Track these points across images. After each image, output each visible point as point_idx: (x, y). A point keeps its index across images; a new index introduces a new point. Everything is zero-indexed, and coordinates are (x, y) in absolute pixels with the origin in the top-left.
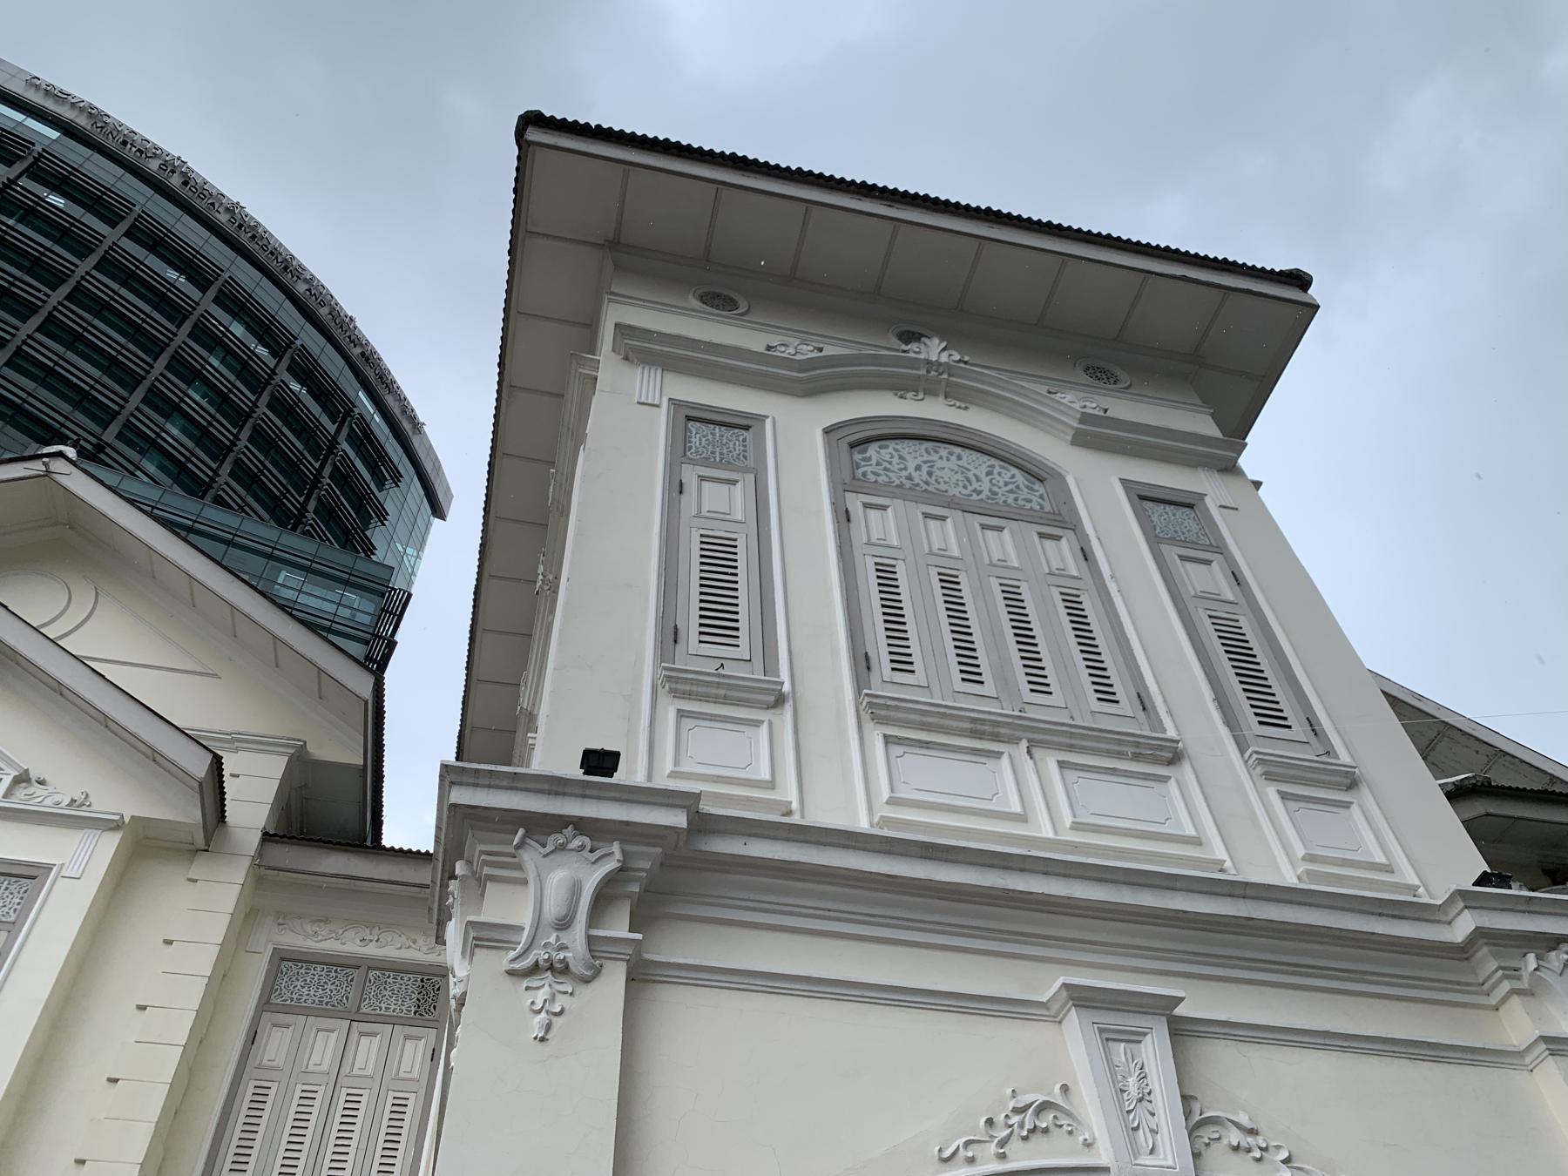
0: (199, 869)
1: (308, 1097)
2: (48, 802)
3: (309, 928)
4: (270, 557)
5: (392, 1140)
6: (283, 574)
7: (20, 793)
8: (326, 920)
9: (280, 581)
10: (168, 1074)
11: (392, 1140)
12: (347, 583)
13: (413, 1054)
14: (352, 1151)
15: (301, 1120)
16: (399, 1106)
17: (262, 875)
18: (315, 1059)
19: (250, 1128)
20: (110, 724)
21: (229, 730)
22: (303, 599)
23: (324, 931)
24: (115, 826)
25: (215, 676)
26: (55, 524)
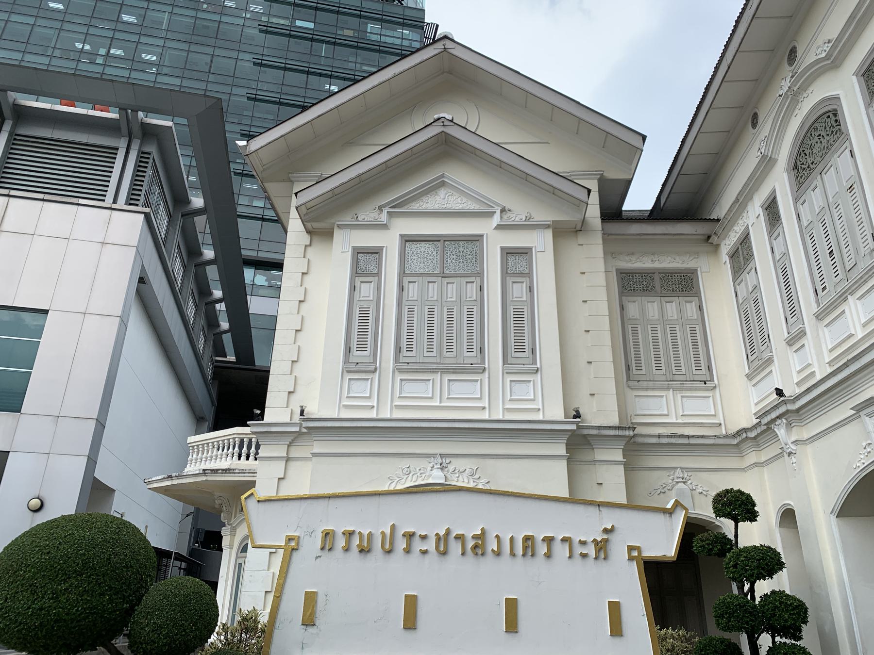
0: (581, 239)
1: (654, 330)
2: (517, 219)
3: (627, 258)
4: (360, 17)
5: (695, 344)
6: (369, 25)
7: (505, 217)
8: (633, 254)
9: (369, 30)
10: (607, 327)
11: (695, 344)
12: (403, 25)
13: (691, 309)
14: (454, 344)
15: (655, 339)
16: (693, 331)
17: (607, 237)
18: (651, 314)
19: (636, 344)
20: (529, 178)
21: (568, 170)
22: (383, 39)
23: (634, 258)
24: (547, 227)
25: (547, 143)
26: (443, 73)
